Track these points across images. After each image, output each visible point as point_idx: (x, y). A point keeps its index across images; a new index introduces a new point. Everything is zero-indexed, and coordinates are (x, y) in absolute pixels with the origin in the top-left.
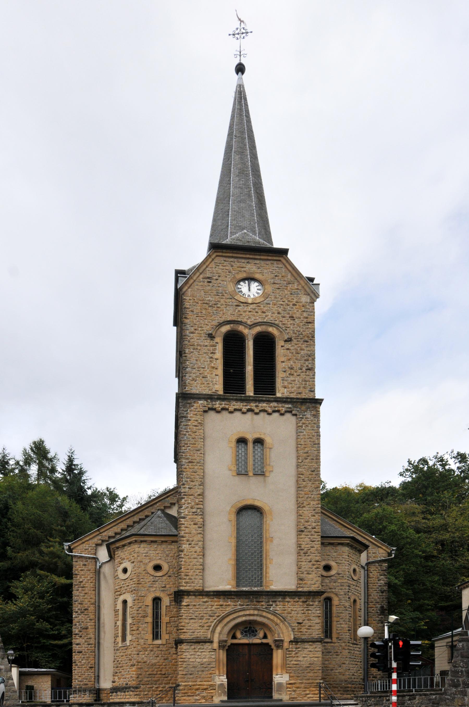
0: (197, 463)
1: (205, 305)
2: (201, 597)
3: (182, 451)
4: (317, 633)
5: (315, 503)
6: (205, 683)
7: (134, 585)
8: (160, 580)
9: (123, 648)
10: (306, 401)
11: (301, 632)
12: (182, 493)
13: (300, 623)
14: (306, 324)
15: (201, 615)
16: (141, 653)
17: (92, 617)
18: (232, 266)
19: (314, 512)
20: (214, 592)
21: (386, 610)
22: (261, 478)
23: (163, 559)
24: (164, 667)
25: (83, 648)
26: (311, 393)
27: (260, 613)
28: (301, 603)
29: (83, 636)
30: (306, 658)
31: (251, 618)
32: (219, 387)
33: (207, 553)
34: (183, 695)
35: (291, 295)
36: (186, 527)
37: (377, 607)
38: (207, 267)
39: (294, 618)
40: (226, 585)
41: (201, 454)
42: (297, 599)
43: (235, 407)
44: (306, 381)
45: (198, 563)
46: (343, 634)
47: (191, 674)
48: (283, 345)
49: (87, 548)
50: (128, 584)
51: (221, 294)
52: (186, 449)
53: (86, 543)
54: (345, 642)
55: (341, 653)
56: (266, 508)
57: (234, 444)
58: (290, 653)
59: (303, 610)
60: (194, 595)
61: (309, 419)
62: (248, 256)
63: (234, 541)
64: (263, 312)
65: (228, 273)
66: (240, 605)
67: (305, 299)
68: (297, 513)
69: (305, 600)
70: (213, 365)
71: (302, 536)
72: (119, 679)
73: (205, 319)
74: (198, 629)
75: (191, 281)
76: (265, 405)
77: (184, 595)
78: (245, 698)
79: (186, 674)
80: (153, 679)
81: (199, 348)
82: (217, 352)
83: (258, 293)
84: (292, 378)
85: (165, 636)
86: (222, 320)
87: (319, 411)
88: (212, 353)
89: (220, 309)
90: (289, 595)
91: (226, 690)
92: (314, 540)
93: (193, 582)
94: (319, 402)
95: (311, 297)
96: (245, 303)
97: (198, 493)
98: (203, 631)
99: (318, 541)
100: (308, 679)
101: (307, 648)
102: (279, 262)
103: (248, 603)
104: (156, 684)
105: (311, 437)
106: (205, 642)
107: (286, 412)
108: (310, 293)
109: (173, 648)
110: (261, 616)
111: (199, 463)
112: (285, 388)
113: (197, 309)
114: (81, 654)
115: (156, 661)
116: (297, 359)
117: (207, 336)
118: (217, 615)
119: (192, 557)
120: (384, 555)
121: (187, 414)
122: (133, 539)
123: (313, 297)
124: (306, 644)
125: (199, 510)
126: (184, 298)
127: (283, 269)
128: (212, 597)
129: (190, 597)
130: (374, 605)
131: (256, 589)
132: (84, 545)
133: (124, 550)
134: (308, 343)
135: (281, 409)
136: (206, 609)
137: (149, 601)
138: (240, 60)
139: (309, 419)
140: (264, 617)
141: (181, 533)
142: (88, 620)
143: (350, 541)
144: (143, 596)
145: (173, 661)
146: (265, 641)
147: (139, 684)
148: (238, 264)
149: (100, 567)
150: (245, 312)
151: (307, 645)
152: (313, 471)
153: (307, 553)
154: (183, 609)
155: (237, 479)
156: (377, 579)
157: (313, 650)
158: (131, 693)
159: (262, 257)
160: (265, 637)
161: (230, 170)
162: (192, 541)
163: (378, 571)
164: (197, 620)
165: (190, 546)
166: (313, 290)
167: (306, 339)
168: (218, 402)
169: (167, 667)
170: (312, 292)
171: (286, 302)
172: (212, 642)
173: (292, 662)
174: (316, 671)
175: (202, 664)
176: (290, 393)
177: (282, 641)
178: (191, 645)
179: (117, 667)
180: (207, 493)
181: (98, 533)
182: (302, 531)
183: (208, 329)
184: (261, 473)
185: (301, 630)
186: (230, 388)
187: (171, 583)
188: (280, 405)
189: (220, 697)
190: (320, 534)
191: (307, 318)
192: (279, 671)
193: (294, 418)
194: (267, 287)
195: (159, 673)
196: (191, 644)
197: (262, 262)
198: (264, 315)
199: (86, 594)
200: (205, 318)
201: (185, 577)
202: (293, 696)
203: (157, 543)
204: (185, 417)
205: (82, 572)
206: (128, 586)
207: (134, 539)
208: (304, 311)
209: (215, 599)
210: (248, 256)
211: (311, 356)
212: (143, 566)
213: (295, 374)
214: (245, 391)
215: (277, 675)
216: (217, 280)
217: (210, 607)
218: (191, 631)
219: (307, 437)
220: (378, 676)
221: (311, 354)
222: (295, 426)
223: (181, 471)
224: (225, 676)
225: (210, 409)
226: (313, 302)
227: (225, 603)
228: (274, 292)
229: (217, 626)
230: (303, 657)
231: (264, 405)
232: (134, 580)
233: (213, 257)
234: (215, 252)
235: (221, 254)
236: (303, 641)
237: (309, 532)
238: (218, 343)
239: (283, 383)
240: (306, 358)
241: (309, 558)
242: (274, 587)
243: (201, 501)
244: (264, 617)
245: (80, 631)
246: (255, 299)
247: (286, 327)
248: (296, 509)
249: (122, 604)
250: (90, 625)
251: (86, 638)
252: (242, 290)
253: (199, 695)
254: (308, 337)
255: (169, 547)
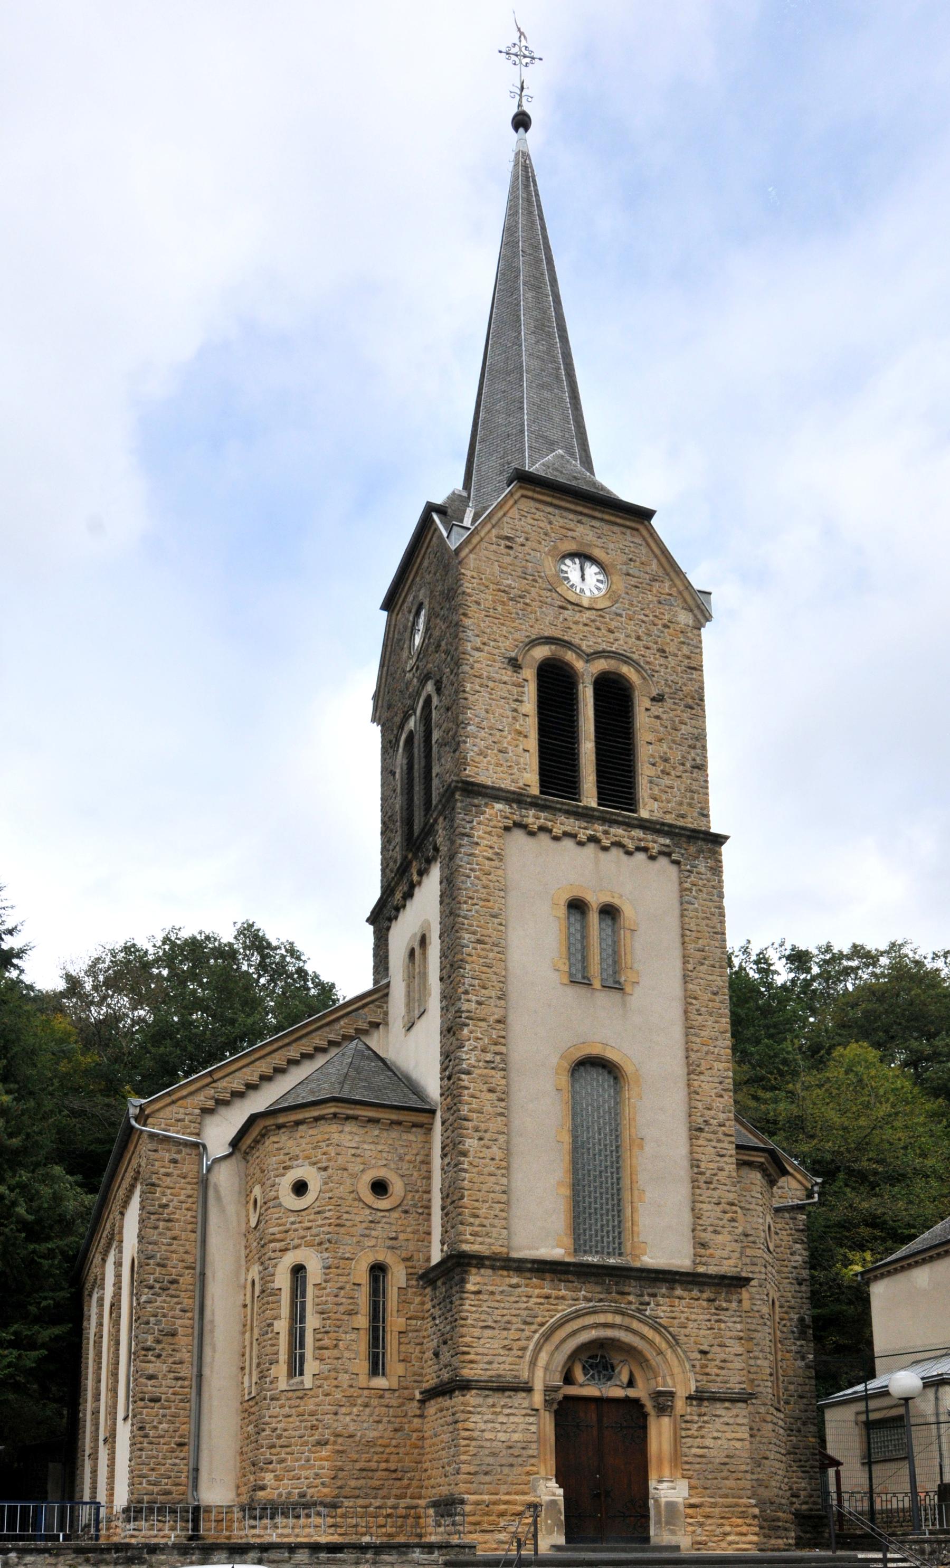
0: (494, 945)
1: (503, 594)
2: (505, 1273)
3: (462, 913)
4: (738, 1379)
5: (721, 1066)
6: (517, 1497)
7: (326, 1229)
8: (384, 1220)
9: (290, 1394)
10: (697, 835)
11: (707, 1374)
12: (462, 1012)
13: (704, 1353)
14: (689, 671)
15: (506, 1318)
16: (343, 1410)
17: (187, 1302)
18: (550, 523)
19: (721, 1087)
20: (534, 1261)
21: (809, 1327)
22: (615, 996)
23: (392, 1166)
24: (393, 1450)
25: (164, 1389)
26: (703, 818)
27: (627, 1321)
28: (705, 1304)
29: (164, 1354)
30: (719, 1442)
31: (609, 1333)
32: (529, 777)
33: (516, 1163)
34: (472, 1528)
35: (660, 606)
36: (473, 1096)
37: (791, 1320)
38: (504, 515)
39: (692, 1339)
40: (553, 1247)
41: (501, 924)
42: (695, 1293)
43: (568, 829)
44: (692, 792)
45: (498, 1188)
46: (761, 1383)
47: (486, 1473)
48: (648, 707)
49: (181, 1116)
50: (309, 1224)
51: (531, 578)
52: (470, 911)
53: (180, 1102)
54: (765, 1404)
55: (759, 1430)
56: (628, 1068)
57: (562, 911)
58: (688, 1425)
59: (709, 1320)
60: (493, 1268)
61: (703, 877)
62: (580, 509)
63: (567, 1138)
64: (611, 631)
65: (543, 537)
66: (587, 1300)
67: (684, 618)
68: (689, 1086)
69: (712, 1296)
70: (518, 727)
71: (701, 1142)
72: (278, 1478)
73: (503, 624)
74: (500, 1355)
75: (475, 540)
76: (620, 831)
77: (469, 1265)
78: (594, 1541)
79: (476, 1473)
80: (370, 1482)
81: (491, 684)
82: (525, 699)
83: (598, 589)
84: (666, 781)
85: (395, 1367)
86: (534, 633)
87: (721, 862)
88: (517, 700)
89: (529, 609)
90: (681, 1283)
91: (563, 1518)
92: (724, 1152)
93: (487, 1234)
94: (719, 840)
95: (695, 616)
96: (577, 605)
97: (496, 1017)
98: (509, 1359)
99: (731, 1156)
100: (726, 1496)
101: (719, 1416)
102: (635, 533)
103: (602, 1296)
104: (375, 1498)
105: (708, 915)
106: (516, 1389)
107: (661, 853)
108: (693, 607)
109: (412, 1399)
110: (628, 1329)
111: (497, 945)
112: (656, 800)
113: (487, 598)
114: (158, 1405)
115: (376, 1434)
116: (674, 742)
117: (506, 661)
118: (539, 1320)
119: (486, 1170)
120: (798, 1193)
121: (472, 828)
122: (330, 1109)
123: (700, 616)
124: (718, 1405)
125: (498, 1058)
126: (463, 571)
127: (642, 548)
128: (528, 1275)
129: (482, 1271)
130: (786, 1313)
131: (612, 1261)
132: (174, 1108)
133: (298, 1135)
134: (694, 712)
135: (651, 845)
136: (516, 1305)
137: (361, 1274)
138: (520, 105)
139: (703, 877)
140: (634, 1332)
141: (462, 1108)
142: (177, 1312)
143: (765, 1157)
144: (348, 1259)
145: (415, 1435)
146: (632, 1393)
147: (337, 1497)
148: (561, 520)
149: (209, 1169)
150: (576, 623)
151: (719, 1408)
152: (715, 994)
153: (711, 1183)
154: (468, 1302)
155: (571, 993)
156: (788, 1251)
157: (731, 1421)
158: (319, 1521)
159: (606, 517)
160: (631, 1383)
161: (518, 316)
162: (486, 1131)
163: (789, 1232)
164: (496, 1332)
165: (482, 1142)
166: (700, 602)
167: (690, 701)
168: (532, 812)
169: (401, 1450)
170: (698, 607)
171: (651, 618)
172: (529, 1390)
173: (694, 1451)
174: (740, 1475)
175: (511, 1447)
176: (665, 813)
177: (671, 1394)
178: (487, 1396)
179: (273, 1446)
180: (511, 1019)
181: (209, 1080)
182: (701, 1130)
183: (507, 646)
184: (615, 986)
185: (707, 1370)
186: (553, 783)
187: (409, 1230)
188: (649, 837)
189: (551, 1539)
190: (733, 1139)
191: (689, 658)
192: (666, 1472)
193: (673, 869)
194: (615, 578)
195: (383, 1465)
196: (487, 1392)
197: (606, 527)
198: (612, 636)
199: (174, 1238)
200: (502, 621)
201: (472, 1220)
202: (699, 1538)
203: (380, 1125)
204: (468, 836)
205: (168, 1179)
206: (309, 1228)
207: (332, 1110)
208: (683, 643)
209: (534, 1280)
210: (580, 509)
211: (698, 740)
212: (348, 1181)
213: (673, 773)
214: (579, 794)
215: (660, 1481)
216: (523, 545)
217: (525, 1299)
218: (486, 1359)
219: (700, 915)
220: (802, 1493)
221: (699, 734)
222: (676, 887)
223: (461, 960)
224: (554, 1480)
225: (519, 825)
226: (698, 627)
227: (554, 1293)
228: (630, 592)
229: (541, 1349)
230: (714, 1438)
231: (618, 832)
232: (327, 1214)
233: (517, 496)
234: (521, 487)
235: (530, 494)
236: (715, 1398)
237: (714, 1133)
238: (527, 681)
239: (651, 789)
240: (690, 742)
241: (716, 1194)
242: (651, 1259)
243: (504, 1037)
244: (634, 1332)
245: (158, 1342)
246: (594, 599)
247: (653, 670)
248: (686, 1077)
249: (289, 1275)
250: (182, 1323)
251: (171, 1360)
252: (569, 575)
253: (504, 1528)
254: (693, 698)
255: (405, 1136)
